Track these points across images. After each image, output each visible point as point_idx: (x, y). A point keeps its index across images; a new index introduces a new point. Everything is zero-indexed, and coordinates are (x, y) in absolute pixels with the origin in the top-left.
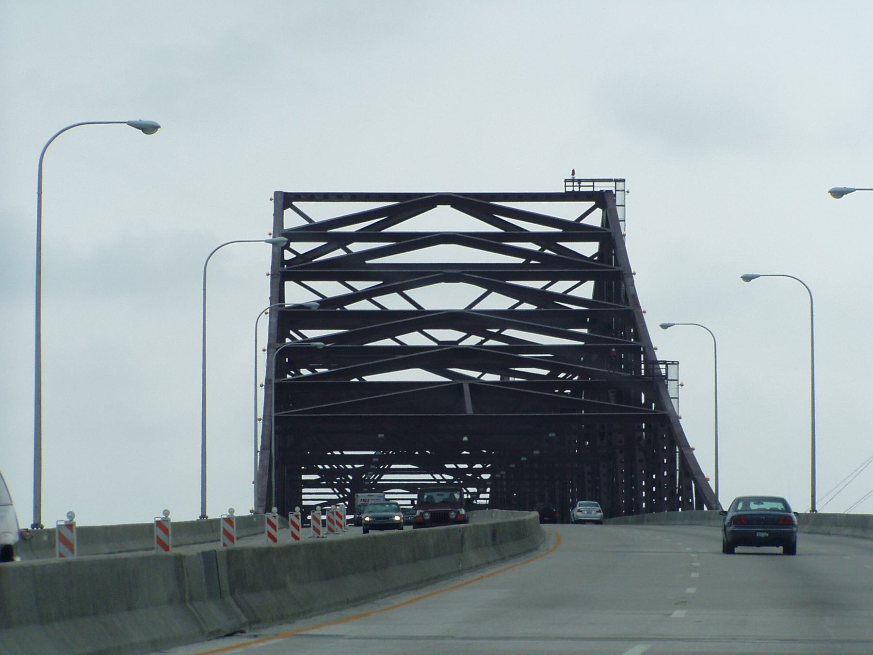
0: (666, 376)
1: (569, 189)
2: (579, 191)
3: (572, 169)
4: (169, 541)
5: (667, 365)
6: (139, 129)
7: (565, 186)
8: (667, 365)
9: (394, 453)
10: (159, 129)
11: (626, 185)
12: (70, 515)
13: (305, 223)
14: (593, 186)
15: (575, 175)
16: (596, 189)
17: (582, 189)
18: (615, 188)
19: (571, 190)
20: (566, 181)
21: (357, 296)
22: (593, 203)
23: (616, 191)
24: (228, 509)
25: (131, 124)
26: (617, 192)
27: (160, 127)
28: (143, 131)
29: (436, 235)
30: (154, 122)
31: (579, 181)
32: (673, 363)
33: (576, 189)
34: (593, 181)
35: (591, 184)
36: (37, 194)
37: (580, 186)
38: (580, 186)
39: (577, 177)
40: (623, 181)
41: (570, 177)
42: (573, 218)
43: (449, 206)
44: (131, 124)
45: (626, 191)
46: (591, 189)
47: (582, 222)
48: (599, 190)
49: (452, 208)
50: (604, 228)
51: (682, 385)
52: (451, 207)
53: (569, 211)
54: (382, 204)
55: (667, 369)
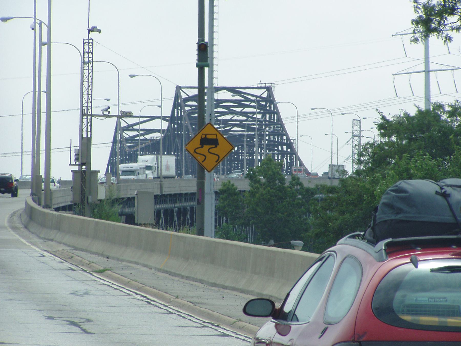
0: (293, 143)
1: (259, 86)
13: (187, 96)
17: (263, 86)
31: (262, 84)
33: (261, 86)
39: (261, 82)
42: (259, 94)
46: (265, 86)
50: (268, 98)
53: (258, 92)
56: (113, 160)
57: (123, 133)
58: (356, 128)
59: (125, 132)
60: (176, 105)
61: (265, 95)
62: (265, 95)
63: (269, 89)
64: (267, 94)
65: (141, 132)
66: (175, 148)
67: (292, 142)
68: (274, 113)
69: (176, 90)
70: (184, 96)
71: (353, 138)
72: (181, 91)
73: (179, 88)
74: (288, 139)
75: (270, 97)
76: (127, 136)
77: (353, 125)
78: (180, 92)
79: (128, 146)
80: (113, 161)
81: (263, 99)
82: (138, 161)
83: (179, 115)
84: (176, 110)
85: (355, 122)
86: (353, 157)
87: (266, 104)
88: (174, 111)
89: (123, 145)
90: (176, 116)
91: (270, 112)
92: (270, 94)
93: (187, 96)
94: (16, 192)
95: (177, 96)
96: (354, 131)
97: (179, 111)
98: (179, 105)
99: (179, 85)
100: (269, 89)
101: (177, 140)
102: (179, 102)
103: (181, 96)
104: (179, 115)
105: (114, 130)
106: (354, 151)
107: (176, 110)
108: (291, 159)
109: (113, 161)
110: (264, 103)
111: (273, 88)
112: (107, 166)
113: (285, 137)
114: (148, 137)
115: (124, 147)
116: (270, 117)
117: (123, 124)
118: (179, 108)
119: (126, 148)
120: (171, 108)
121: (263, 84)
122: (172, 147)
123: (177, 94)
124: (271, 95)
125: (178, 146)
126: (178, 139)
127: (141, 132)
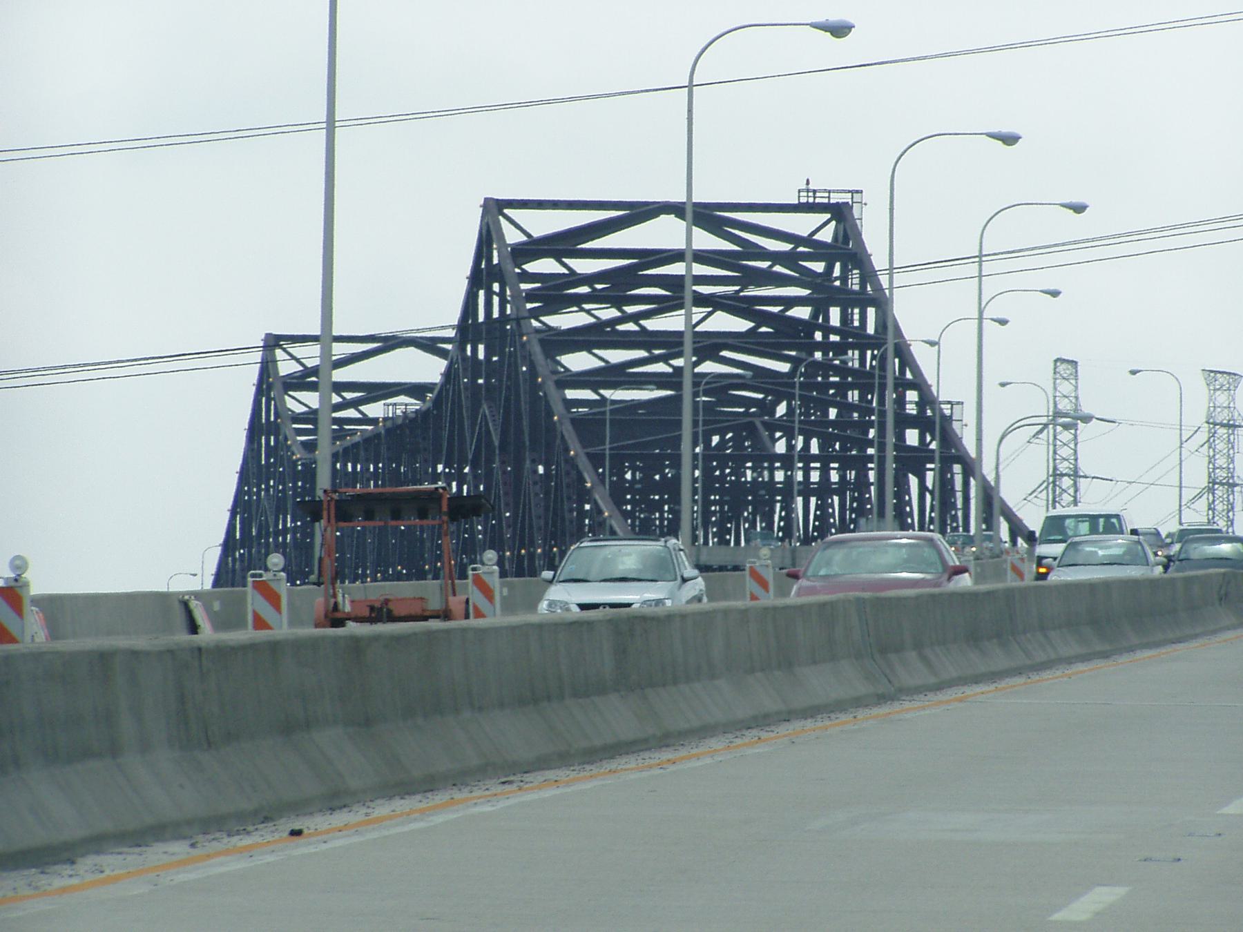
0: (951, 417)
1: (803, 200)
2: (814, 203)
3: (806, 179)
4: (253, 596)
5: (952, 405)
6: (826, 31)
7: (799, 197)
8: (952, 405)
9: (767, 497)
10: (853, 29)
11: (864, 197)
12: (18, 562)
13: (524, 238)
14: (829, 197)
15: (810, 186)
16: (832, 201)
17: (818, 200)
18: (852, 200)
19: (805, 201)
20: (799, 191)
21: (626, 318)
22: (828, 216)
23: (853, 203)
24: (8, 560)
25: (815, 26)
26: (854, 204)
27: (854, 27)
28: (832, 34)
29: (671, 253)
30: (845, 21)
31: (815, 192)
32: (958, 403)
33: (811, 200)
34: (829, 192)
35: (827, 195)
36: (686, 120)
37: (815, 198)
38: (815, 198)
39: (811, 187)
40: (861, 192)
41: (804, 187)
42: (804, 233)
43: (673, 216)
44: (815, 26)
45: (863, 202)
46: (826, 201)
47: (815, 237)
48: (835, 202)
49: (676, 219)
50: (840, 245)
51: (966, 425)
52: (676, 216)
53: (802, 224)
54: (611, 214)
55: (952, 409)
56: (249, 493)
57: (286, 397)
58: (1065, 387)
59: (291, 393)
60: (480, 277)
61: (826, 235)
62: (826, 235)
63: (840, 213)
64: (834, 227)
65: (349, 395)
66: (479, 440)
67: (947, 412)
68: (863, 301)
69: (483, 217)
70: (513, 236)
71: (1055, 425)
72: (503, 222)
73: (495, 208)
74: (927, 399)
75: (846, 239)
76: (299, 409)
77: (1055, 379)
78: (499, 221)
79: (303, 443)
80: (250, 497)
81: (820, 250)
82: (293, 837)
83: (496, 315)
84: (482, 293)
85: (1062, 367)
86: (1055, 485)
87: (829, 269)
88: (476, 296)
89: (286, 439)
90: (481, 318)
91: (848, 300)
92: (845, 230)
93: (524, 238)
94: (818, 516)
95: (488, 237)
96: (1057, 399)
97: (496, 300)
98: (496, 273)
99: (496, 197)
100: (840, 213)
101: (485, 408)
102: (495, 261)
103: (501, 236)
104: (496, 315)
105: (254, 389)
106: (1059, 466)
107: (482, 293)
108: (945, 485)
109: (250, 497)
110: (819, 267)
111: (856, 208)
112: (228, 514)
113: (912, 396)
114: (375, 410)
115: (289, 448)
116: (845, 318)
117: (286, 367)
118: (496, 287)
119: (296, 451)
120: (463, 286)
121: (818, 194)
122: (467, 434)
123: (489, 231)
124: (849, 232)
125: (488, 432)
126: (489, 407)
127: (349, 395)
